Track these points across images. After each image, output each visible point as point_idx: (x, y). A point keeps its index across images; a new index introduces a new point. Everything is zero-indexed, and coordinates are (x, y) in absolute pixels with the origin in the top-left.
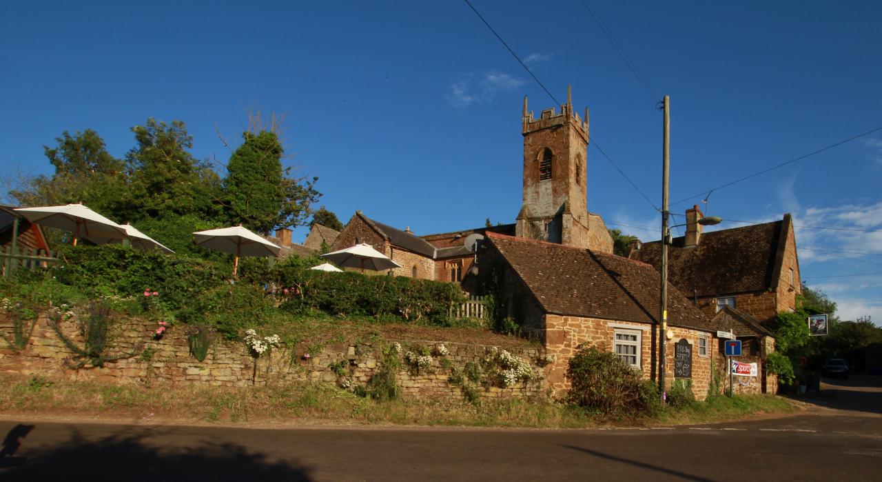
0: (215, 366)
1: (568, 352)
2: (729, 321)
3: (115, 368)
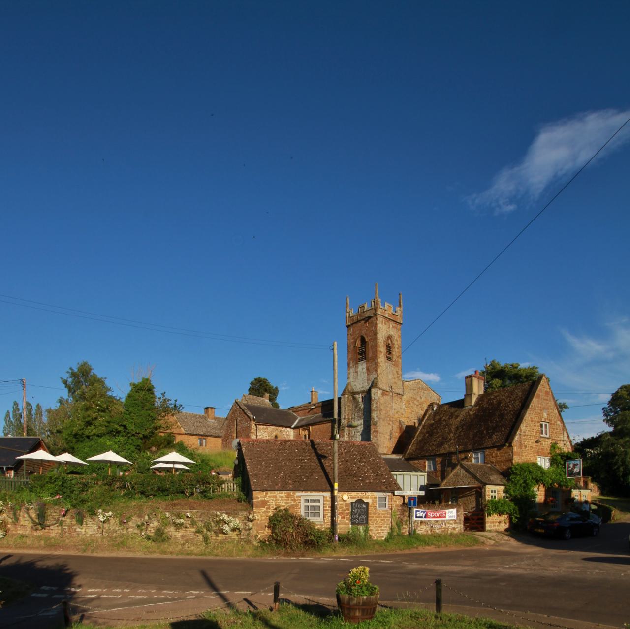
0: (87, 527)
1: (269, 512)
2: (463, 474)
3: (50, 529)
